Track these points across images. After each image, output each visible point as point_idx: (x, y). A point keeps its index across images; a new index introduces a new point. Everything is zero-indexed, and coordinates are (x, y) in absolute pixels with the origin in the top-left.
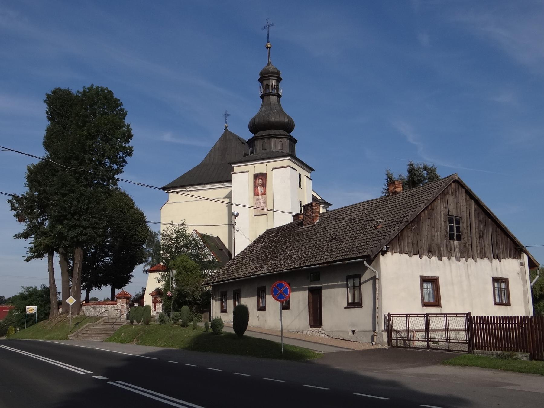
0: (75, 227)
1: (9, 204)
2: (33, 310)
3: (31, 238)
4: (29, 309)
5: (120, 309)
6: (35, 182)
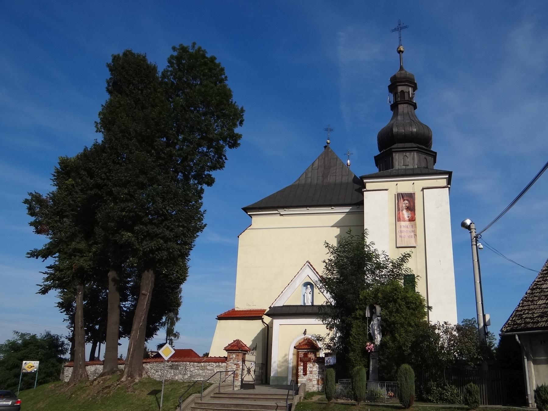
0: (151, 236)
1: (27, 205)
2: (34, 366)
3: (53, 257)
4: (27, 366)
5: (232, 370)
6: (83, 171)
